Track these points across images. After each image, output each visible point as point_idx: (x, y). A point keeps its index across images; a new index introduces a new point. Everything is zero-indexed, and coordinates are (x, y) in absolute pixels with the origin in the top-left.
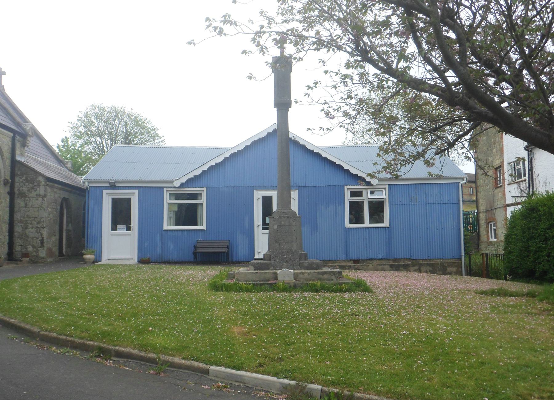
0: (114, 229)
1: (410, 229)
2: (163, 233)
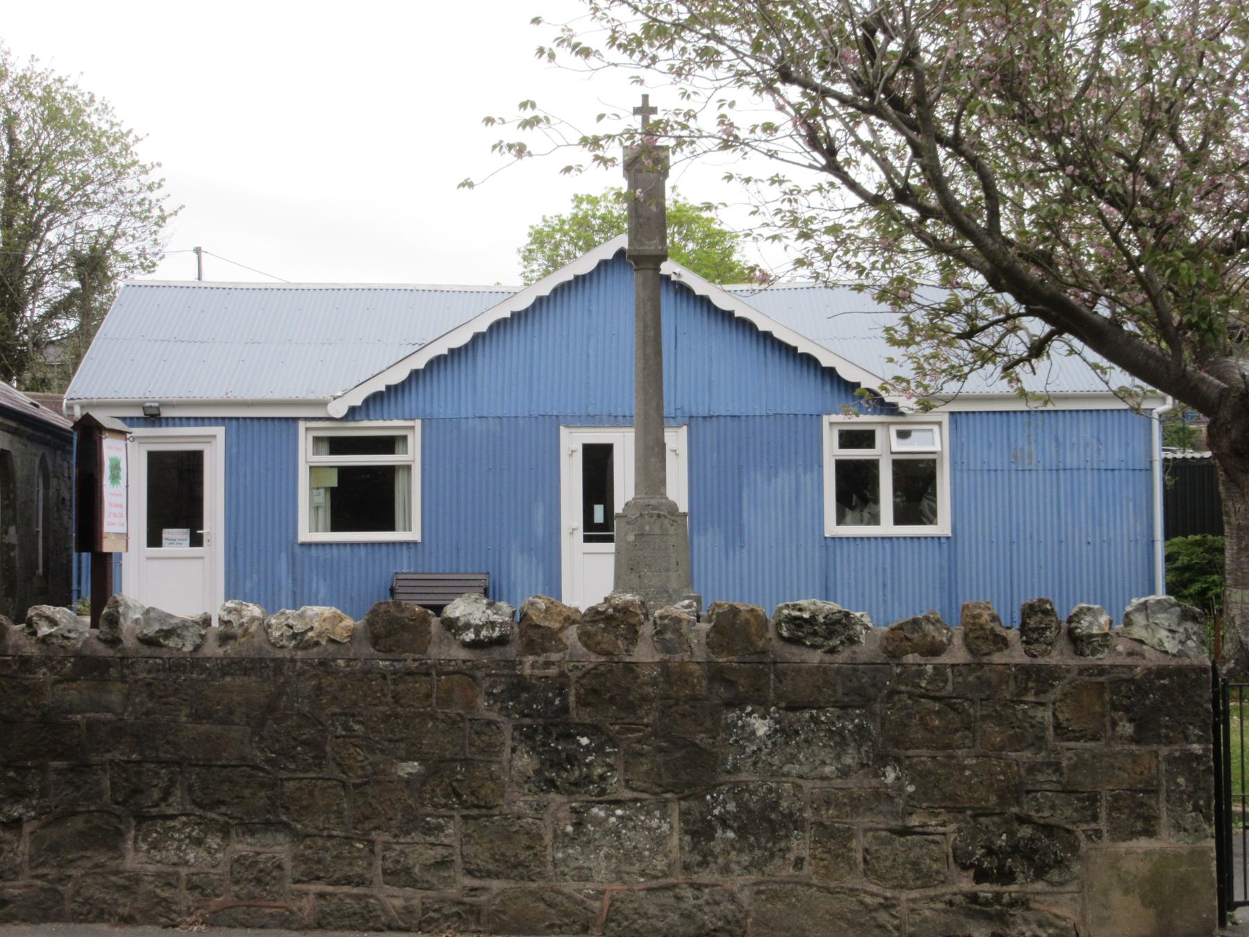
0: (154, 540)
1: (1012, 543)
2: (298, 551)
